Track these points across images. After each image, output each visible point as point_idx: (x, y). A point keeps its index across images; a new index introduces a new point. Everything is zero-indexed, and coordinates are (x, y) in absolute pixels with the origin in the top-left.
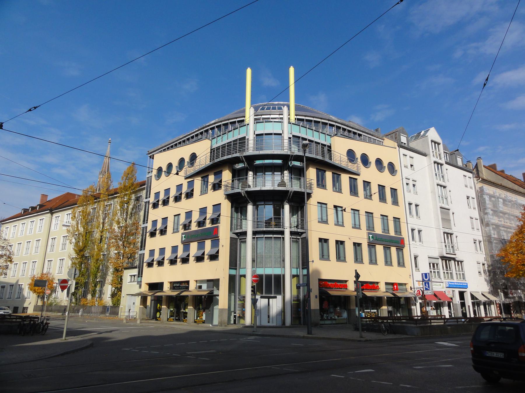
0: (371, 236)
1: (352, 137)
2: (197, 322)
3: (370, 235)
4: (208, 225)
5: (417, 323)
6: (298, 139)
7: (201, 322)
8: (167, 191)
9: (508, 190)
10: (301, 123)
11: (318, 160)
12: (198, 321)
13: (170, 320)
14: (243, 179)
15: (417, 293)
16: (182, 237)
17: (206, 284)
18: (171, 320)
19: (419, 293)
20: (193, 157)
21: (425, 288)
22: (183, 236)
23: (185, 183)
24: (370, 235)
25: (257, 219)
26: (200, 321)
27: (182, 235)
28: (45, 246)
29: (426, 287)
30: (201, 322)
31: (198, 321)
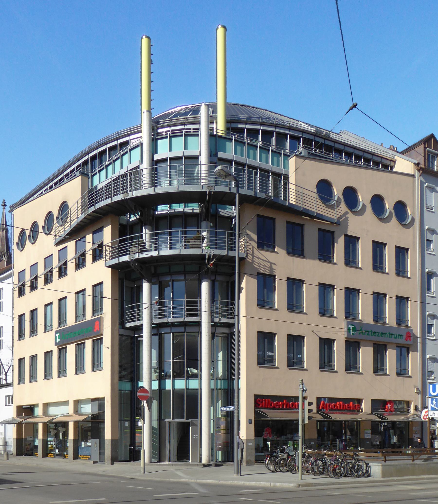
0: (352, 327)
1: (324, 156)
2: (82, 458)
3: (350, 326)
4: (89, 316)
5: (387, 459)
6: (230, 164)
7: (87, 458)
8: (34, 266)
9: (114, 135)
10: (236, 136)
11: (258, 201)
12: (83, 457)
13: (50, 456)
14: (135, 238)
15: (425, 415)
16: (56, 337)
17: (90, 405)
18: (51, 456)
19: (427, 416)
20: (64, 207)
21: (431, 407)
22: (58, 335)
23: (55, 250)
24: (350, 326)
25: (173, 304)
26: (85, 457)
27: (55, 334)
28: (146, 368)
29: (433, 406)
30: (87, 458)
31: (83, 457)
